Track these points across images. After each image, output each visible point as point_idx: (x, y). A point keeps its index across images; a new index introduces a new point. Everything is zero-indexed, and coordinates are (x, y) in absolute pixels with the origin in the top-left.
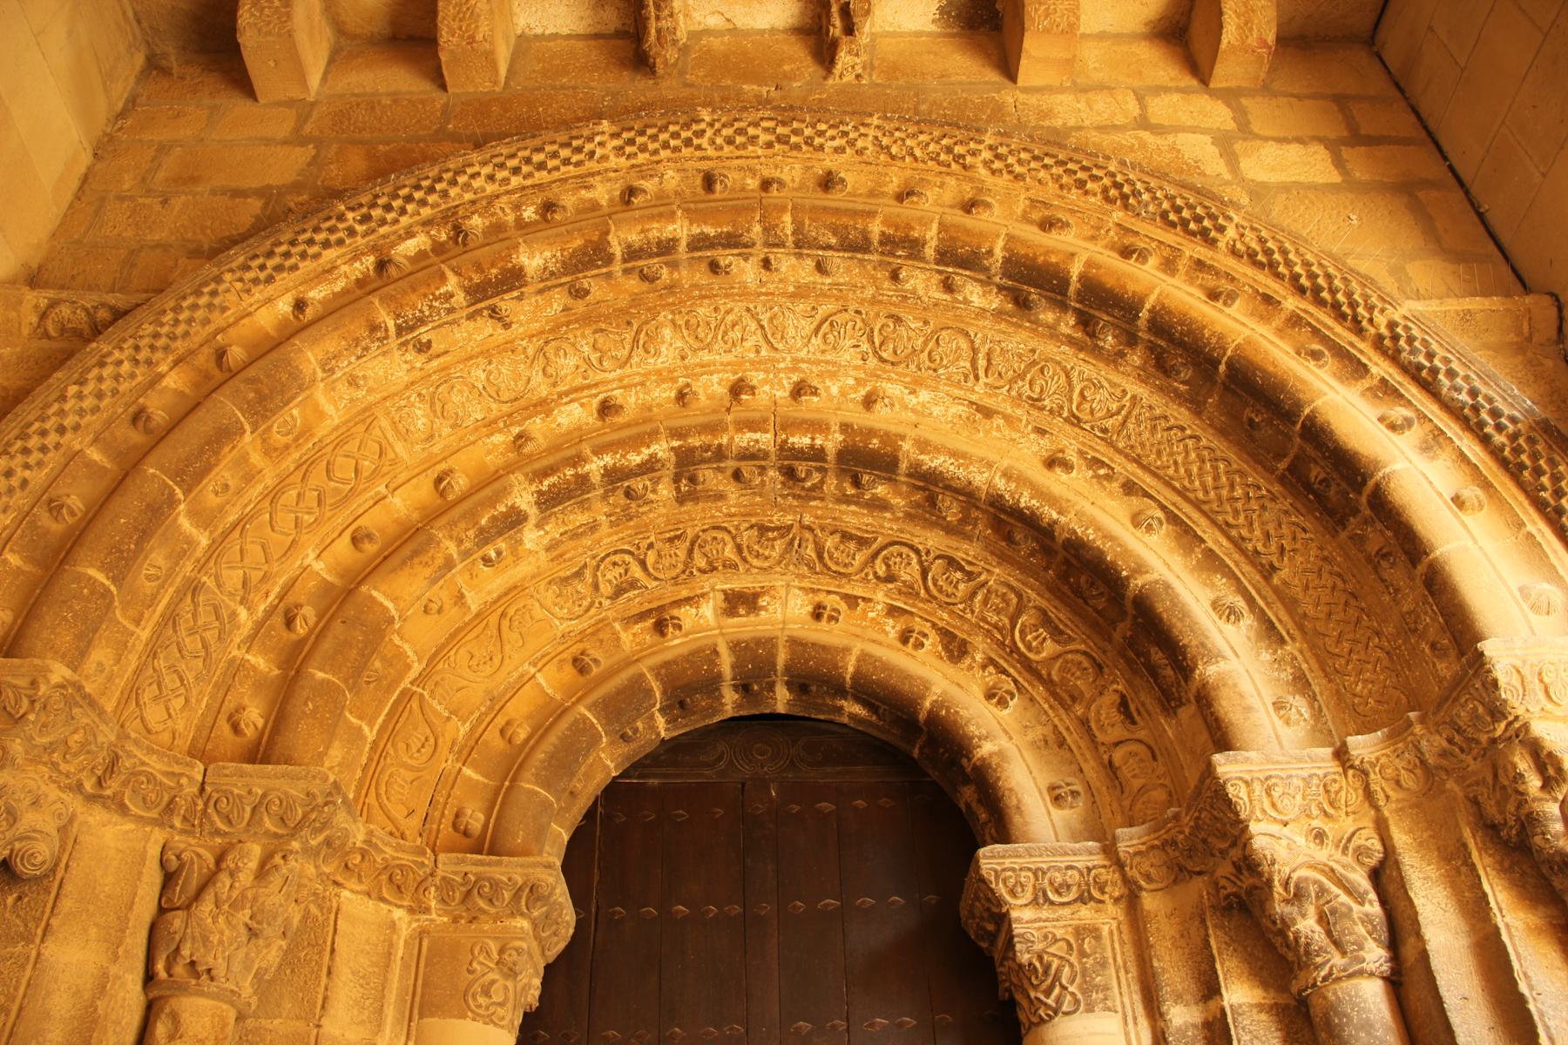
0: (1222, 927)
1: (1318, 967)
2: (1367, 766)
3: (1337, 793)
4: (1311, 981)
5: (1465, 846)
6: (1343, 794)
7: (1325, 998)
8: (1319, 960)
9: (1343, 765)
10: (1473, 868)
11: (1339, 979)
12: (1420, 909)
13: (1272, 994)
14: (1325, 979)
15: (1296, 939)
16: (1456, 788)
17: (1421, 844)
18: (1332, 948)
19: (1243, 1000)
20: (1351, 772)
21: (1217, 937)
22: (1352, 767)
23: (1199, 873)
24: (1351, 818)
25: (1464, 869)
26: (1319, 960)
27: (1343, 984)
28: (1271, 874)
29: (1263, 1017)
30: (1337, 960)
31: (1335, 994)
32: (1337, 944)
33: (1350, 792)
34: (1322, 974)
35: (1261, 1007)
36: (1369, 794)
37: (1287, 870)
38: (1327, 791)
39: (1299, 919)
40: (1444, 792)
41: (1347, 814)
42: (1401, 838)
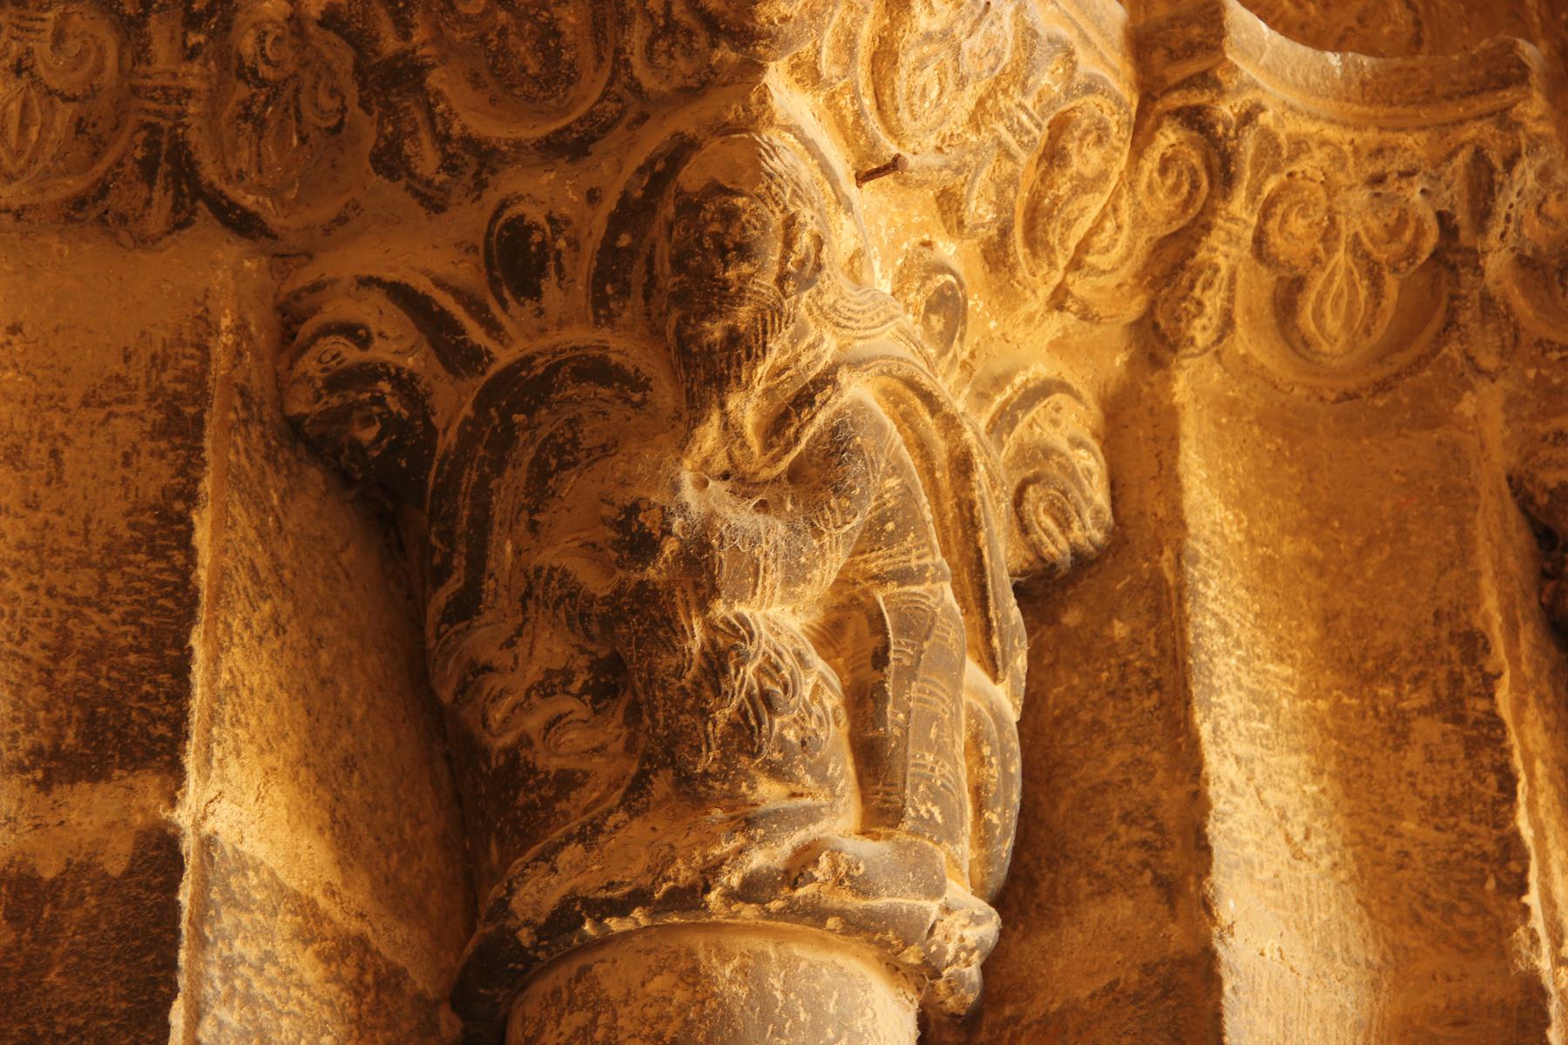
0: (257, 503)
1: (747, 821)
2: (1248, 146)
3: (1084, 186)
4: (682, 873)
5: (1474, 644)
6: (1095, 204)
7: (693, 976)
8: (769, 792)
9: (1149, 90)
10: (1490, 731)
11: (815, 914)
12: (1217, 792)
13: (359, 895)
14: (753, 889)
15: (717, 664)
16: (1496, 429)
17: (1267, 567)
18: (843, 767)
19: (256, 848)
20: (1169, 137)
21: (222, 524)
22: (1196, 119)
23: (244, 224)
24: (1055, 324)
25: (1428, 729)
26: (769, 792)
27: (805, 954)
28: (771, 317)
29: (308, 966)
30: (840, 823)
31: (752, 973)
32: (872, 758)
33: (1114, 210)
34: (758, 860)
35: (311, 926)
36: (1172, 264)
37: (830, 347)
38: (1053, 156)
39: (774, 577)
40: (1434, 421)
41: (1059, 300)
42: (1211, 504)
